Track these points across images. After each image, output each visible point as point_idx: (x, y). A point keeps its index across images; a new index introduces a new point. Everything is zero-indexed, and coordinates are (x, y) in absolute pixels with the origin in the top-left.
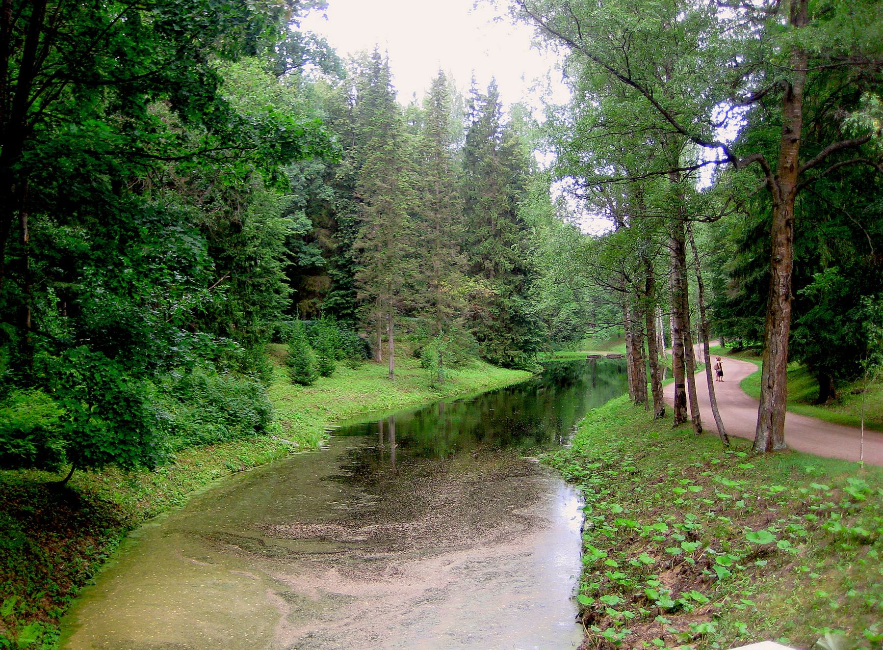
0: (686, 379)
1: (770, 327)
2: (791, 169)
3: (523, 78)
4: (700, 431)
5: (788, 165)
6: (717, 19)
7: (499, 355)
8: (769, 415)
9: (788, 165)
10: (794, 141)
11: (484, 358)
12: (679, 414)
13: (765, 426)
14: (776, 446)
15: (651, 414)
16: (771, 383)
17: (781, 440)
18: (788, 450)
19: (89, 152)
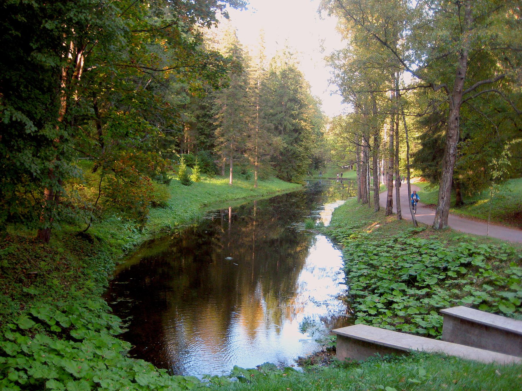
0: (422, 215)
1: (444, 169)
2: (460, 92)
3: (311, 59)
4: (401, 219)
5: (458, 90)
6: (41, 23)
7: (285, 175)
8: (441, 212)
9: (458, 90)
10: (462, 79)
11: (277, 177)
12: (389, 210)
13: (439, 217)
14: (444, 227)
15: (373, 210)
16: (443, 196)
17: (446, 224)
18: (449, 229)
19: (38, 287)
